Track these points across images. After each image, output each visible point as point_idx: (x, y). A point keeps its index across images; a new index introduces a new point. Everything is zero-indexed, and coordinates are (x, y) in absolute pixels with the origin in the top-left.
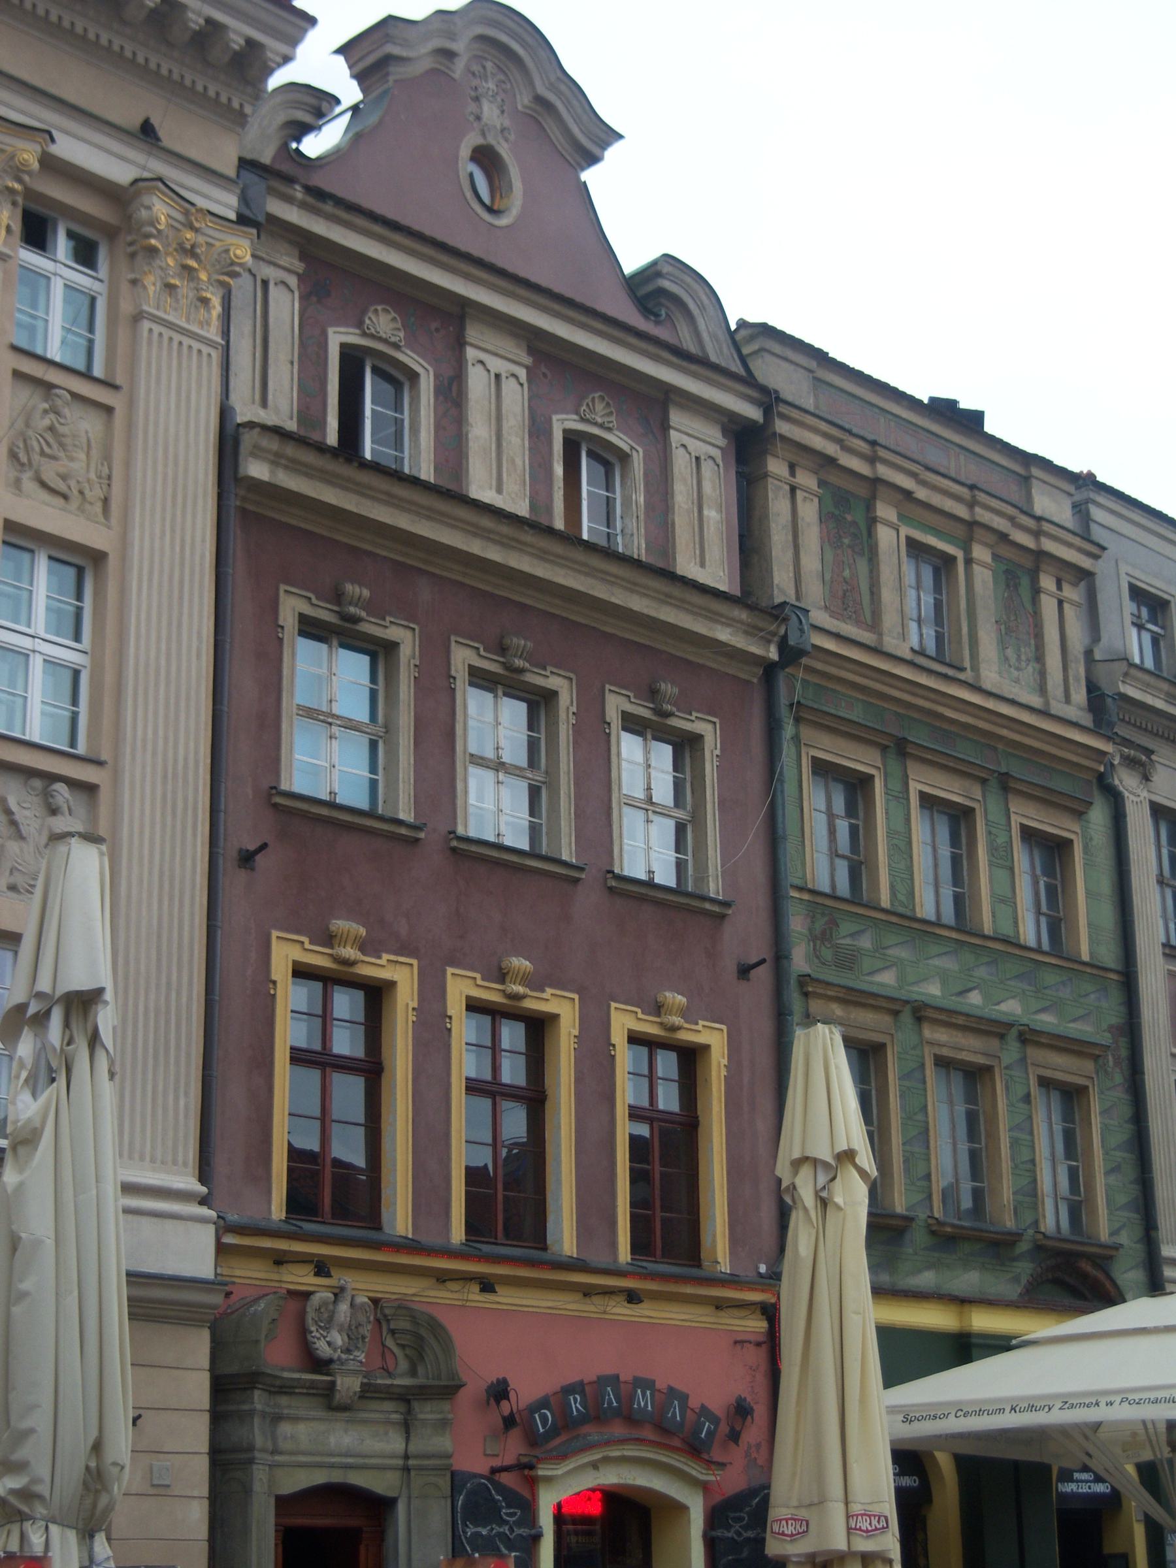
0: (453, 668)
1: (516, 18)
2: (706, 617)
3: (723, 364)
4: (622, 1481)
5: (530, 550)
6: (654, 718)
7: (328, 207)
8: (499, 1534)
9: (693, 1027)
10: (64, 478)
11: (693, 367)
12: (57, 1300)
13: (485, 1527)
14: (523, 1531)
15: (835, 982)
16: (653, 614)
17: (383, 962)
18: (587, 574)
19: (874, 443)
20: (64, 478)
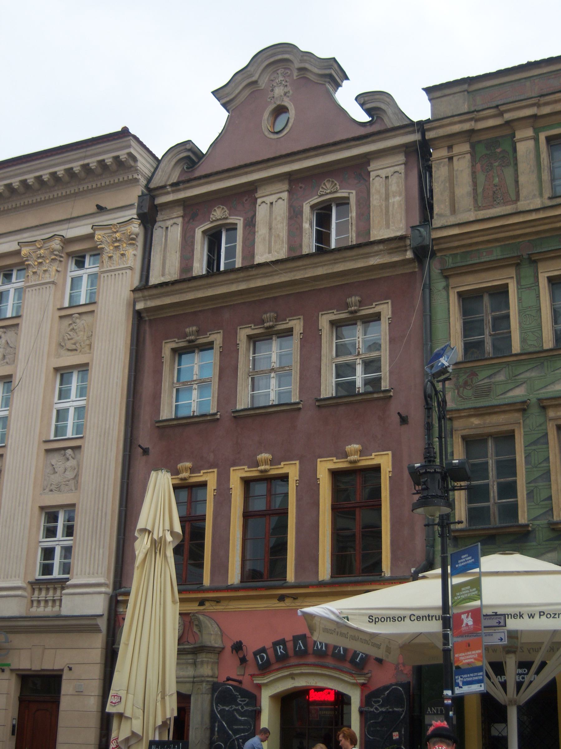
0: (163, 354)
2: (363, 258)
3: (401, 124)
4: (308, 685)
5: (372, 254)
6: (349, 316)
7: (181, 186)
8: (235, 710)
9: (199, 474)
10: (75, 344)
11: (370, 139)
13: (227, 706)
14: (250, 708)
15: (502, 403)
16: (330, 271)
17: (373, 457)
18: (290, 272)
19: (497, 107)
20: (75, 344)
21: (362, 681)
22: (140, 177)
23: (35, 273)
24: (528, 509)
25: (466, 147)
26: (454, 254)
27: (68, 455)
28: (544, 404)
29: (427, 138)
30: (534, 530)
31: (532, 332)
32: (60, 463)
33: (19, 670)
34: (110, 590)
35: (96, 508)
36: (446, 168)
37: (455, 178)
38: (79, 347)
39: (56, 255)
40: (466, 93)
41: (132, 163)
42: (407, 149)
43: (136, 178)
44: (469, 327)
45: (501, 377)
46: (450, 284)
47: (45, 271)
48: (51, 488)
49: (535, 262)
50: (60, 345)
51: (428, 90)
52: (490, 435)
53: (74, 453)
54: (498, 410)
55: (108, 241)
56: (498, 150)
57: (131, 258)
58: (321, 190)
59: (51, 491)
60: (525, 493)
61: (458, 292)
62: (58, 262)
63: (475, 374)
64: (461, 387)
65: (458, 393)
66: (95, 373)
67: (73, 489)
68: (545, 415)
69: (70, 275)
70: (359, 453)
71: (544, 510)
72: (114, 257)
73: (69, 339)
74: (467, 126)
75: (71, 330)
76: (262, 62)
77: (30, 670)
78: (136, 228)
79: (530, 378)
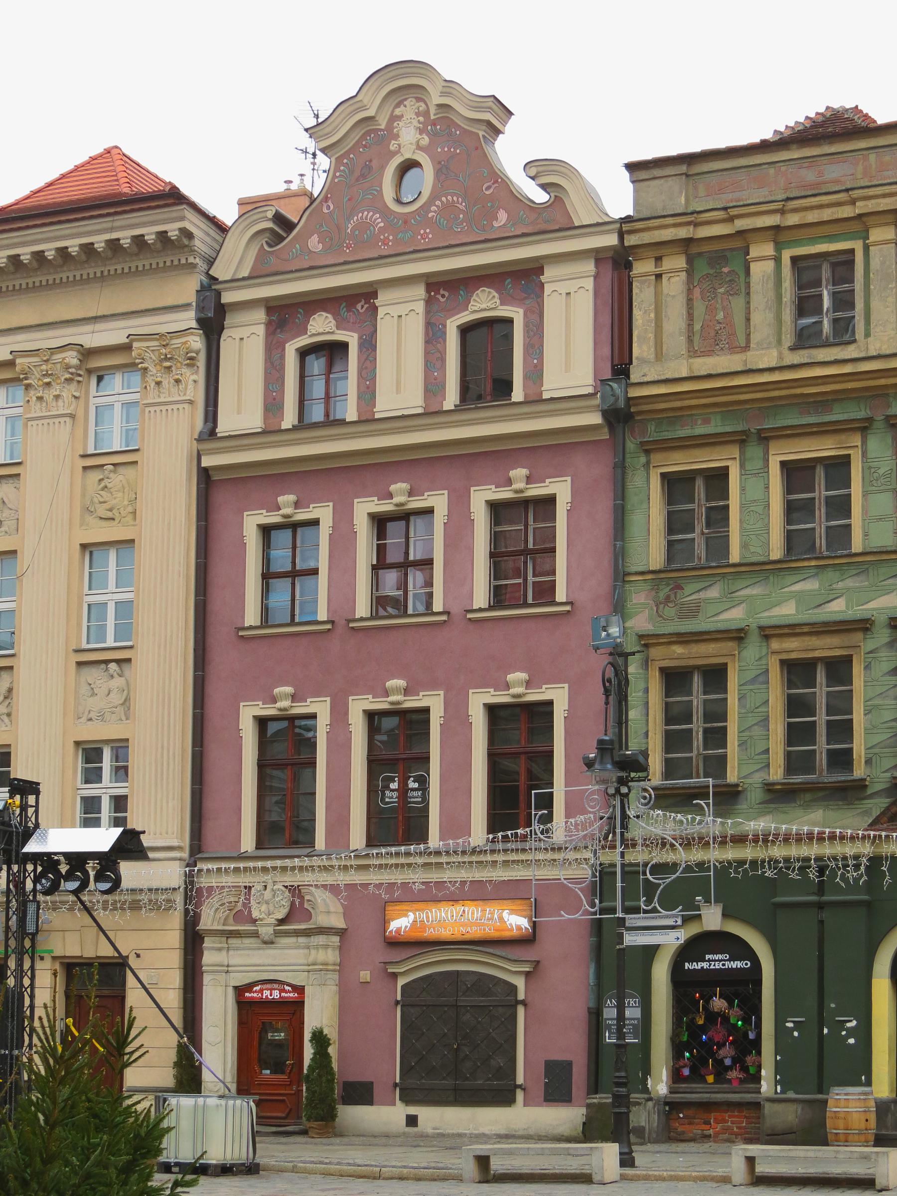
1: (403, 66)
10: (110, 510)
12: (444, 1179)
19: (725, 209)
20: (110, 510)
21: (528, 969)
22: (198, 260)
23: (40, 399)
24: (739, 764)
25: (680, 262)
26: (659, 419)
27: (111, 671)
28: (767, 633)
29: (626, 244)
30: (745, 790)
31: (757, 535)
32: (100, 682)
33: (65, 957)
34: (185, 855)
35: (160, 745)
36: (652, 289)
37: (663, 299)
38: (117, 515)
39: (72, 374)
40: (684, 177)
41: (186, 241)
42: (598, 256)
43: (192, 263)
44: (676, 524)
45: (714, 593)
46: (652, 461)
47: (57, 397)
48: (90, 716)
49: (767, 439)
50: (87, 510)
51: (632, 167)
52: (697, 668)
53: (121, 669)
54: (708, 637)
55: (154, 358)
56: (726, 270)
57: (191, 385)
58: (472, 303)
59: (90, 719)
60: (736, 744)
61: (661, 474)
62: (75, 383)
63: (679, 587)
64: (661, 603)
65: (657, 611)
66: (145, 552)
67: (124, 718)
68: (768, 647)
69: (93, 402)
70: (525, 684)
71: (760, 766)
72: (165, 383)
73: (101, 503)
74: (683, 233)
75: (103, 489)
76: (380, 88)
77: (81, 957)
78: (197, 342)
79: (748, 596)
